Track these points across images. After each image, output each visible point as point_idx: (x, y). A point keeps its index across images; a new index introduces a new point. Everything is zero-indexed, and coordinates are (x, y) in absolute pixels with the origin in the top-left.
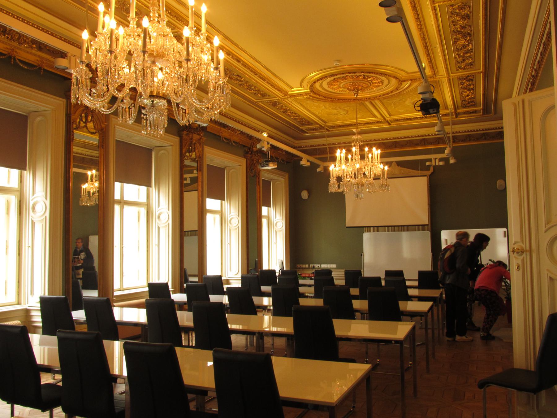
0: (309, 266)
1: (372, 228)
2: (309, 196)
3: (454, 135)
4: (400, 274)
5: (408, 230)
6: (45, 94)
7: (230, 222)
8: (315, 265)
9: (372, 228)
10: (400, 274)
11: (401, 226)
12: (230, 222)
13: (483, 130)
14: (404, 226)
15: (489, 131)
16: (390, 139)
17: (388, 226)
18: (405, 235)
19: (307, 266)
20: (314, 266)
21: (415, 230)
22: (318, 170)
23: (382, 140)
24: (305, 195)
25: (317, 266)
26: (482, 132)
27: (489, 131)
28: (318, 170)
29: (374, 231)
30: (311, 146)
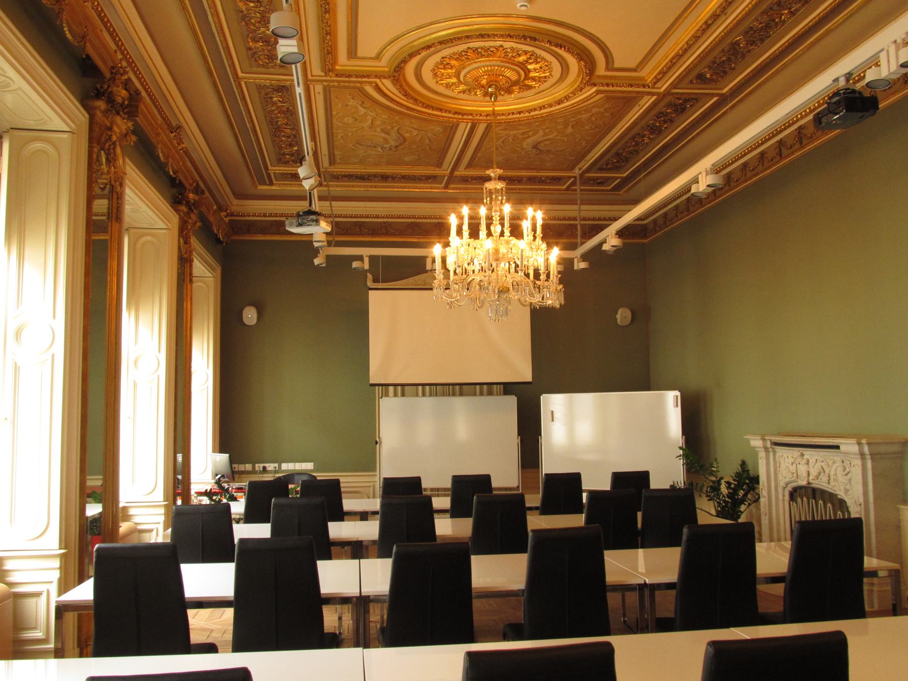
0: (254, 467)
1: (391, 388)
2: (258, 319)
3: (582, 222)
4: (415, 483)
5: (461, 394)
6: (19, 35)
7: (136, 362)
8: (267, 465)
9: (391, 388)
10: (415, 483)
11: (449, 385)
12: (136, 362)
13: (594, 219)
14: (454, 385)
15: (368, 220)
16: (346, 217)
17: (424, 385)
18: (459, 403)
19: (249, 467)
20: (264, 468)
21: (475, 395)
22: (316, 262)
23: (414, 217)
24: (250, 316)
25: (271, 467)
26: (385, 220)
27: (368, 220)
28: (316, 262)
29: (395, 395)
30: (265, 215)
